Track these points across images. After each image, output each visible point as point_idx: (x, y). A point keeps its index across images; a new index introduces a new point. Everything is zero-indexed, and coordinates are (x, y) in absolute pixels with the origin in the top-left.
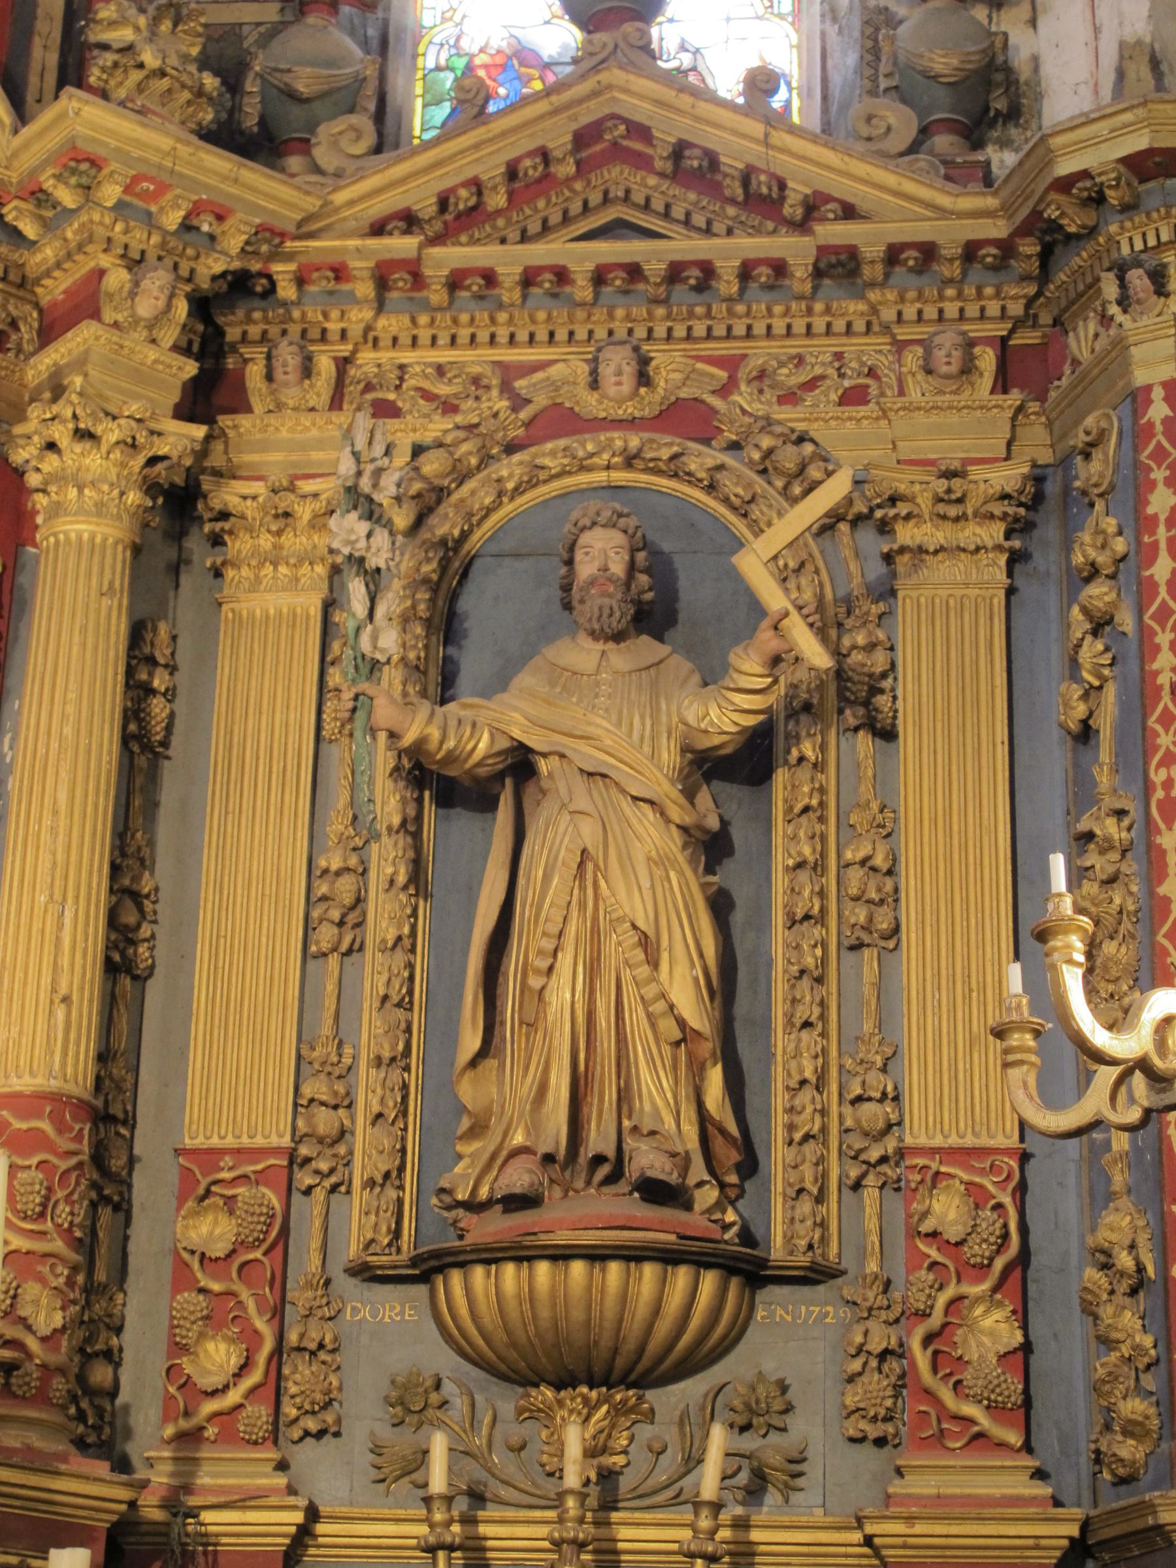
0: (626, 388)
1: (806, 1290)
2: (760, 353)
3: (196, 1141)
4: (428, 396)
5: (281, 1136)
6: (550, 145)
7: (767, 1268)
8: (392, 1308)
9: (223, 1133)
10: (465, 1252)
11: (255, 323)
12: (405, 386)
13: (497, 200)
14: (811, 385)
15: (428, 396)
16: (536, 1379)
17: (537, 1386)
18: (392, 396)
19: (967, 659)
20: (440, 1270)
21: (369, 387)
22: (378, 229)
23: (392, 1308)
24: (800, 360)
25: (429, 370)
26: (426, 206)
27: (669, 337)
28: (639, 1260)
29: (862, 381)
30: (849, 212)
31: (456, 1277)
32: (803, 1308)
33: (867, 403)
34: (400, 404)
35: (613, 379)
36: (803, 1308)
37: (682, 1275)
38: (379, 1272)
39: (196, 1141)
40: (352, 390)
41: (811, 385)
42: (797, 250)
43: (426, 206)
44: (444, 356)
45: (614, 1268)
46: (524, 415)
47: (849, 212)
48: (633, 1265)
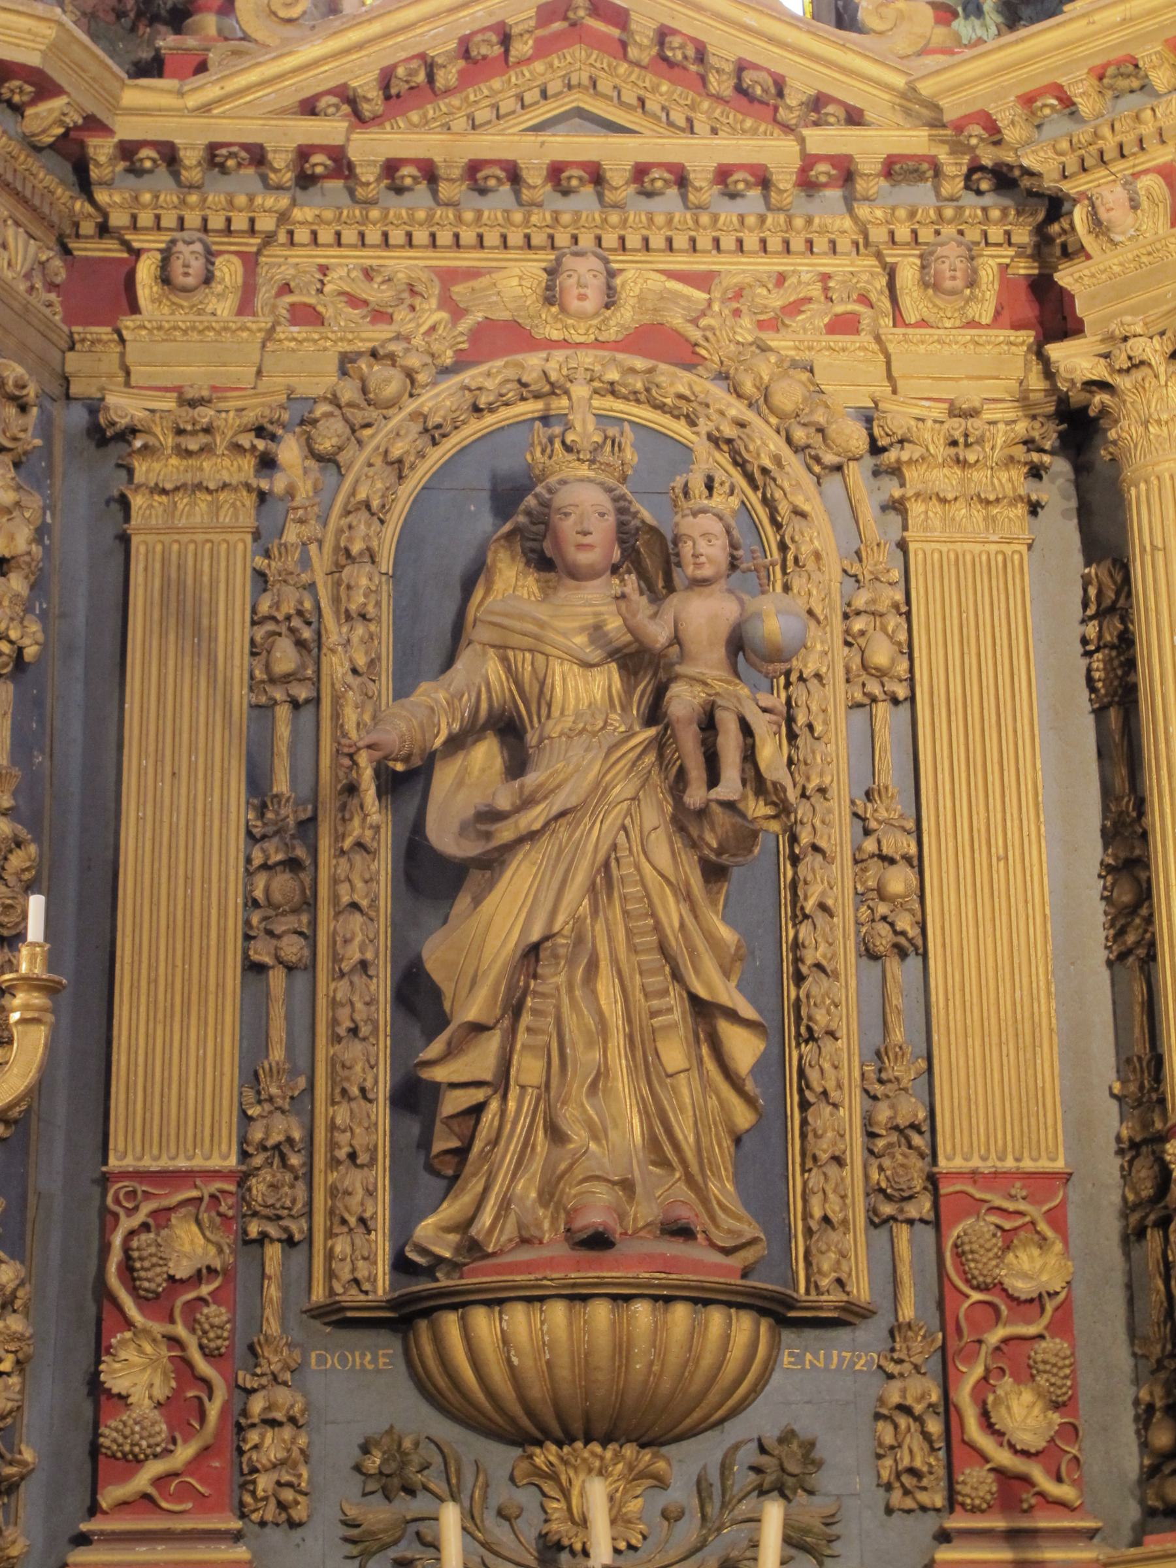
0: (589, 306)
1: (843, 1334)
2: (735, 269)
3: (125, 1163)
4: (354, 301)
5: (226, 1157)
6: (510, 21)
7: (792, 1308)
8: (363, 1356)
9: (138, 1154)
10: (821, 1308)
11: (145, 207)
12: (327, 289)
13: (447, 77)
14: (795, 308)
15: (354, 301)
16: (538, 1435)
17: (540, 1444)
18: (311, 300)
19: (223, 564)
20: (427, 1313)
21: (286, 289)
22: (309, 108)
23: (363, 1356)
24: (781, 279)
25: (354, 274)
26: (365, 82)
27: (647, 246)
28: (706, 1302)
29: (850, 307)
30: (854, 118)
31: (450, 1322)
32: (835, 1353)
33: (857, 332)
34: (320, 308)
35: (575, 292)
36: (835, 1353)
37: (716, 1317)
38: (349, 1314)
39: (125, 1163)
40: (265, 294)
41: (795, 308)
42: (778, 153)
43: (365, 82)
44: (369, 257)
45: (680, 1313)
46: (465, 325)
47: (854, 118)
48: (733, 1311)
